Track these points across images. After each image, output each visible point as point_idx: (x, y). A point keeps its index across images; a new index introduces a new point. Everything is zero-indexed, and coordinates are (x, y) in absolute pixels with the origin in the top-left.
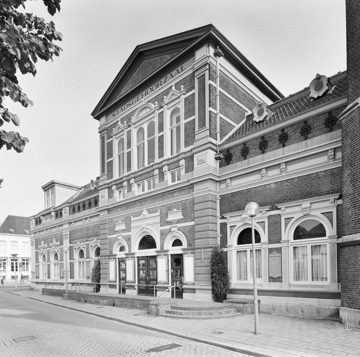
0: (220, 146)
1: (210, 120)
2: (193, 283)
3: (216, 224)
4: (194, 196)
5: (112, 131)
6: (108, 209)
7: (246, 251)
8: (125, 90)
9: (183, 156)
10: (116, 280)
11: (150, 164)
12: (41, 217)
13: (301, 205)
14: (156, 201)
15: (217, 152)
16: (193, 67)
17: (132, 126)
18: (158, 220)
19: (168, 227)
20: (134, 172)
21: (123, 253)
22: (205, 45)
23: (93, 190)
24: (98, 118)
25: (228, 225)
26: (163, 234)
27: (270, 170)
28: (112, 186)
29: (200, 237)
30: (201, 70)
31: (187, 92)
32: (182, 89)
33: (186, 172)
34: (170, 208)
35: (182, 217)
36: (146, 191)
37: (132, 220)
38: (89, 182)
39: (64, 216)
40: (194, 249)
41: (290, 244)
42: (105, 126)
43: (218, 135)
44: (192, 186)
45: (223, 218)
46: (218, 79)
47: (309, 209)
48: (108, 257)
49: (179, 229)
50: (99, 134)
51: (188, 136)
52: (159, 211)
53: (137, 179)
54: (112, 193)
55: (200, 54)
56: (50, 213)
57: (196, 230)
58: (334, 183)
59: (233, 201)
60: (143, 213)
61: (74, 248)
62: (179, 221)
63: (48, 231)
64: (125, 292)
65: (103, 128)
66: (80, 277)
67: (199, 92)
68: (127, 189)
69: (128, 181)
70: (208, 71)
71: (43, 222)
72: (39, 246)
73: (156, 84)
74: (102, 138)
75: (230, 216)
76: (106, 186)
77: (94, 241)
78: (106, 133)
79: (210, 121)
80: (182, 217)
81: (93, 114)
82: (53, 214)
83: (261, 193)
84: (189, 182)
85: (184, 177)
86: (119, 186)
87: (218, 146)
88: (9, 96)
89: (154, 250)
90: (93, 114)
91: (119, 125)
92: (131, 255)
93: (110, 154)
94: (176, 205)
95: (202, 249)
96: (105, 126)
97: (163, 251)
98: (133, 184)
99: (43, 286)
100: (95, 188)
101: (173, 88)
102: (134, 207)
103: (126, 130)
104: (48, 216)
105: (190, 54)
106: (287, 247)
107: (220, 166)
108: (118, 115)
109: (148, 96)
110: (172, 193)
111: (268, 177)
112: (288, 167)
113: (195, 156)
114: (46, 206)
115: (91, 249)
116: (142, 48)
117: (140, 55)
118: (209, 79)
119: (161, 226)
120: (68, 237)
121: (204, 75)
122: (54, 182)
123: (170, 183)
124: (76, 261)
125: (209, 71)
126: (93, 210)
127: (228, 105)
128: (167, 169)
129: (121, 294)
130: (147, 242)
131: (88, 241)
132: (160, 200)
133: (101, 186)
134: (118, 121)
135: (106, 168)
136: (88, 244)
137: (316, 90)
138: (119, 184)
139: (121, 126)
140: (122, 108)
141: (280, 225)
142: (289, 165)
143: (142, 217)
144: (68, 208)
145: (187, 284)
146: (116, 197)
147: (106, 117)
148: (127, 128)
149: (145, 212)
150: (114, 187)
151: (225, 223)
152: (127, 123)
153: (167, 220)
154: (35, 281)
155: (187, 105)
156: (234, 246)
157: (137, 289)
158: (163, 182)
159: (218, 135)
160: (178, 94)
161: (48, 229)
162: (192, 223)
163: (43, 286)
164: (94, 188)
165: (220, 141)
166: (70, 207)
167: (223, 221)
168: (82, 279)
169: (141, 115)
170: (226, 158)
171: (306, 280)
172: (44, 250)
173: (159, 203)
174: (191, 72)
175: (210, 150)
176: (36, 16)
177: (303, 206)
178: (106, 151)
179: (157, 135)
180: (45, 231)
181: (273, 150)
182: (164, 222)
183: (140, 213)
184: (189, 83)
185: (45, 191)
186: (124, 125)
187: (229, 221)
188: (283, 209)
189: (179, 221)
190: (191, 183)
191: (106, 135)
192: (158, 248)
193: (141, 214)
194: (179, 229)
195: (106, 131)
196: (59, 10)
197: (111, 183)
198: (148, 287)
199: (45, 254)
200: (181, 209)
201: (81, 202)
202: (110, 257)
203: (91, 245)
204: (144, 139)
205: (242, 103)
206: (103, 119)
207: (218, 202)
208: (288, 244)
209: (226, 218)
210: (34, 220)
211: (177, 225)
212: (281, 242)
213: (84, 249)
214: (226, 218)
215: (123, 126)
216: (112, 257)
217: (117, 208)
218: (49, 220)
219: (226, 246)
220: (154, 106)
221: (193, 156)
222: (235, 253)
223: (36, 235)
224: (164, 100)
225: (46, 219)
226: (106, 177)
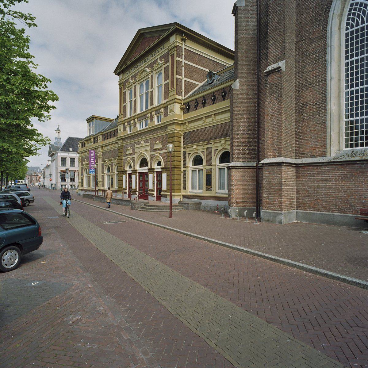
0: (183, 100)
1: (177, 83)
3: (180, 152)
6: (122, 139)
7: (196, 170)
9: (163, 106)
10: (154, 189)
11: (97, 131)
12: (85, 142)
15: (182, 104)
17: (154, 71)
20: (155, 106)
21: (159, 167)
22: (175, 34)
24: (118, 74)
27: (191, 123)
28: (152, 112)
33: (164, 117)
34: (155, 139)
35: (161, 147)
36: (144, 127)
39: (98, 141)
41: (216, 166)
42: (122, 81)
43: (183, 93)
46: (184, 56)
49: (160, 154)
52: (150, 142)
53: (139, 119)
55: (173, 39)
56: (90, 139)
60: (142, 143)
62: (160, 149)
63: (112, 146)
64: (161, 200)
65: (172, 46)
66: (194, 187)
67: (171, 65)
69: (151, 113)
70: (176, 51)
71: (86, 145)
72: (84, 163)
73: (150, 55)
74: (120, 89)
75: (214, 142)
76: (122, 122)
78: (123, 85)
79: (177, 84)
80: (162, 146)
82: (92, 140)
85: (164, 120)
86: (129, 123)
89: (147, 168)
91: (158, 62)
92: (135, 171)
93: (125, 101)
96: (122, 81)
99: (83, 193)
103: (150, 75)
104: (89, 141)
105: (167, 39)
107: (184, 114)
108: (130, 74)
109: (145, 63)
111: (189, 127)
112: (216, 117)
113: (168, 106)
114: (89, 134)
115: (214, 155)
116: (142, 31)
117: (142, 36)
118: (177, 57)
119: (151, 152)
120: (101, 157)
121: (174, 54)
122: (93, 116)
123: (156, 123)
124: (106, 174)
125: (177, 52)
126: (113, 139)
127: (192, 71)
128: (154, 114)
133: (119, 122)
134: (129, 78)
135: (122, 109)
138: (129, 121)
139: (160, 63)
140: (158, 50)
142: (216, 116)
144: (101, 136)
146: (127, 131)
147: (123, 74)
148: (164, 65)
150: (154, 113)
154: (81, 189)
155: (165, 72)
156: (190, 167)
158: (125, 131)
159: (183, 93)
161: (112, 144)
163: (83, 193)
166: (102, 135)
168: (197, 190)
169: (142, 75)
170: (187, 108)
171: (222, 189)
173: (150, 136)
174: (167, 51)
175: (176, 104)
178: (122, 98)
179: (150, 90)
180: (110, 145)
181: (209, 105)
183: (139, 143)
184: (165, 57)
185: (88, 122)
187: (187, 150)
188: (213, 144)
189: (160, 149)
194: (160, 154)
195: (122, 84)
198: (144, 194)
199: (109, 166)
201: (109, 132)
203: (189, 153)
204: (143, 92)
205: (206, 68)
206: (121, 75)
207: (182, 137)
209: (211, 144)
210: (81, 143)
211: (159, 152)
213: (204, 155)
214: (211, 144)
216: (124, 172)
218: (90, 144)
222: (217, 170)
223: (82, 154)
225: (88, 143)
226: (122, 116)
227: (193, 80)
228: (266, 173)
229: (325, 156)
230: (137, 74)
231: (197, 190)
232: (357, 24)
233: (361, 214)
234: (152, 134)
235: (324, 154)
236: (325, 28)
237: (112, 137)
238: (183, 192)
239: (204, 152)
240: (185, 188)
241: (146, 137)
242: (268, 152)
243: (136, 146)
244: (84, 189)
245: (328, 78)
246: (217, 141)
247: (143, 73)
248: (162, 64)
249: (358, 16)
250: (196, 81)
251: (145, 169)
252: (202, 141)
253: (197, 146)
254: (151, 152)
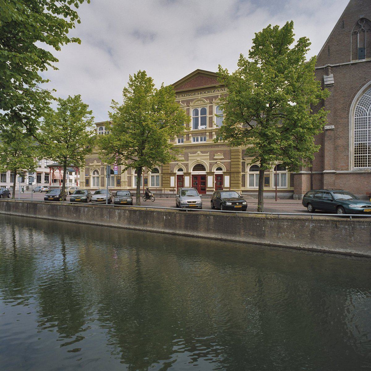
26: (211, 165)
34: (217, 152)
40: (231, 173)
45: (244, 159)
52: (209, 153)
62: (221, 159)
66: (94, 185)
88: (148, 77)
92: (188, 174)
97: (211, 173)
129: (128, 175)
130: (200, 167)
143: (196, 154)
153: (214, 158)
162: (230, 161)
167: (243, 161)
169: (197, 103)
176: (69, 96)
182: (212, 158)
196: (305, 37)
228: (326, 177)
229: (348, 170)
230: (192, 100)
231: (155, 187)
232: (360, 116)
233: (366, 194)
235: (347, 169)
236: (348, 114)
238: (243, 189)
240: (244, 185)
242: (326, 167)
244: (91, 188)
245: (350, 136)
247: (199, 102)
249: (360, 112)
251: (181, 173)
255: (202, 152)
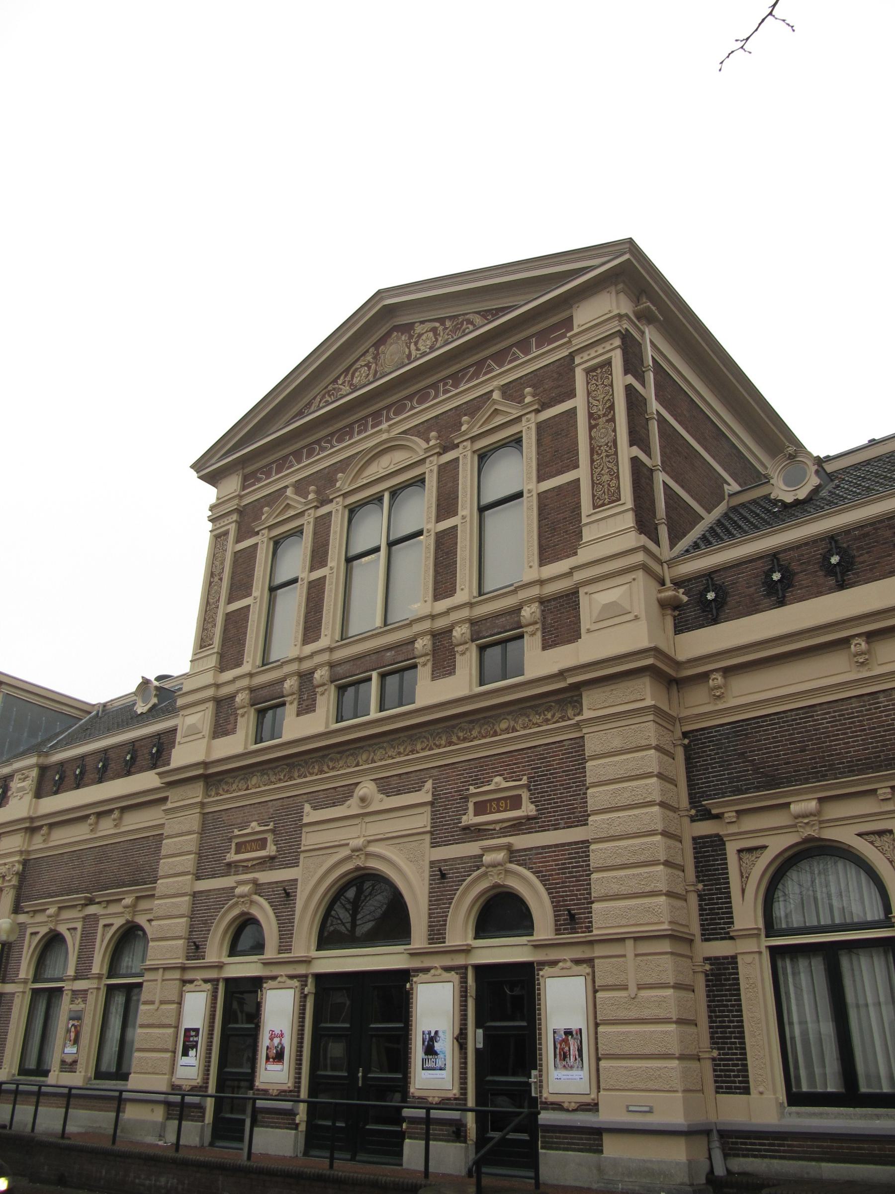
2: (586, 1099)
4: (585, 731)
5: (257, 517)
8: (364, 381)
13: (789, 804)
14: (296, 774)
16: (570, 342)
18: (422, 820)
19: (471, 849)
23: (142, 713)
24: (212, 478)
25: (727, 844)
26: (443, 877)
28: (237, 692)
29: (615, 888)
30: (603, 345)
31: (544, 406)
32: (528, 399)
34: (480, 770)
37: (306, 820)
38: (131, 686)
44: (577, 693)
45: (706, 815)
47: (816, 818)
48: (177, 975)
50: (211, 524)
51: (554, 529)
52: (429, 785)
54: (232, 718)
57: (595, 860)
58: (858, 741)
59: (743, 753)
60: (360, 791)
61: (29, 931)
68: (296, 703)
77: (48, 912)
81: (197, 466)
83: (859, 721)
84: (565, 679)
87: (665, 565)
90: (197, 466)
91: (287, 498)
94: (506, 763)
95: (630, 944)
98: (323, 685)
100: (154, 706)
101: (496, 395)
102: (321, 772)
106: (757, 956)
110: (490, 717)
119: (434, 845)
126: (146, 780)
130: (365, 905)
131: (99, 903)
132: (435, 744)
134: (286, 487)
136: (95, 914)
137: (787, 484)
141: (586, 889)
143: (352, 807)
145: (558, 1107)
149: (367, 788)
151: (717, 835)
152: (317, 492)
157: (303, 1127)
160: (300, 507)
164: (149, 706)
165: (671, 549)
167: (705, 828)
169: (367, 472)
172: (66, 915)
177: (795, 808)
186: (428, 442)
187: (733, 829)
190: (571, 680)
191: (233, 528)
192: (419, 937)
193: (350, 795)
197: (447, 612)
200: (525, 778)
202: (189, 976)
206: (233, 484)
208: (759, 947)
209: (718, 817)
212: (732, 934)
214: (718, 817)
215: (426, 446)
217: (245, 771)
219: (728, 933)
220: (424, 445)
221: (578, 592)
223: (38, 842)
224: (338, 485)
227: (683, 487)
234: (451, 743)
237: (110, 773)
239: (75, 929)
241: (396, 762)
243: (310, 815)
246: (766, 797)
248: (306, 504)
250: (692, 496)
252: (852, 772)
253: (821, 800)
254: (434, 845)
255: (386, 787)
